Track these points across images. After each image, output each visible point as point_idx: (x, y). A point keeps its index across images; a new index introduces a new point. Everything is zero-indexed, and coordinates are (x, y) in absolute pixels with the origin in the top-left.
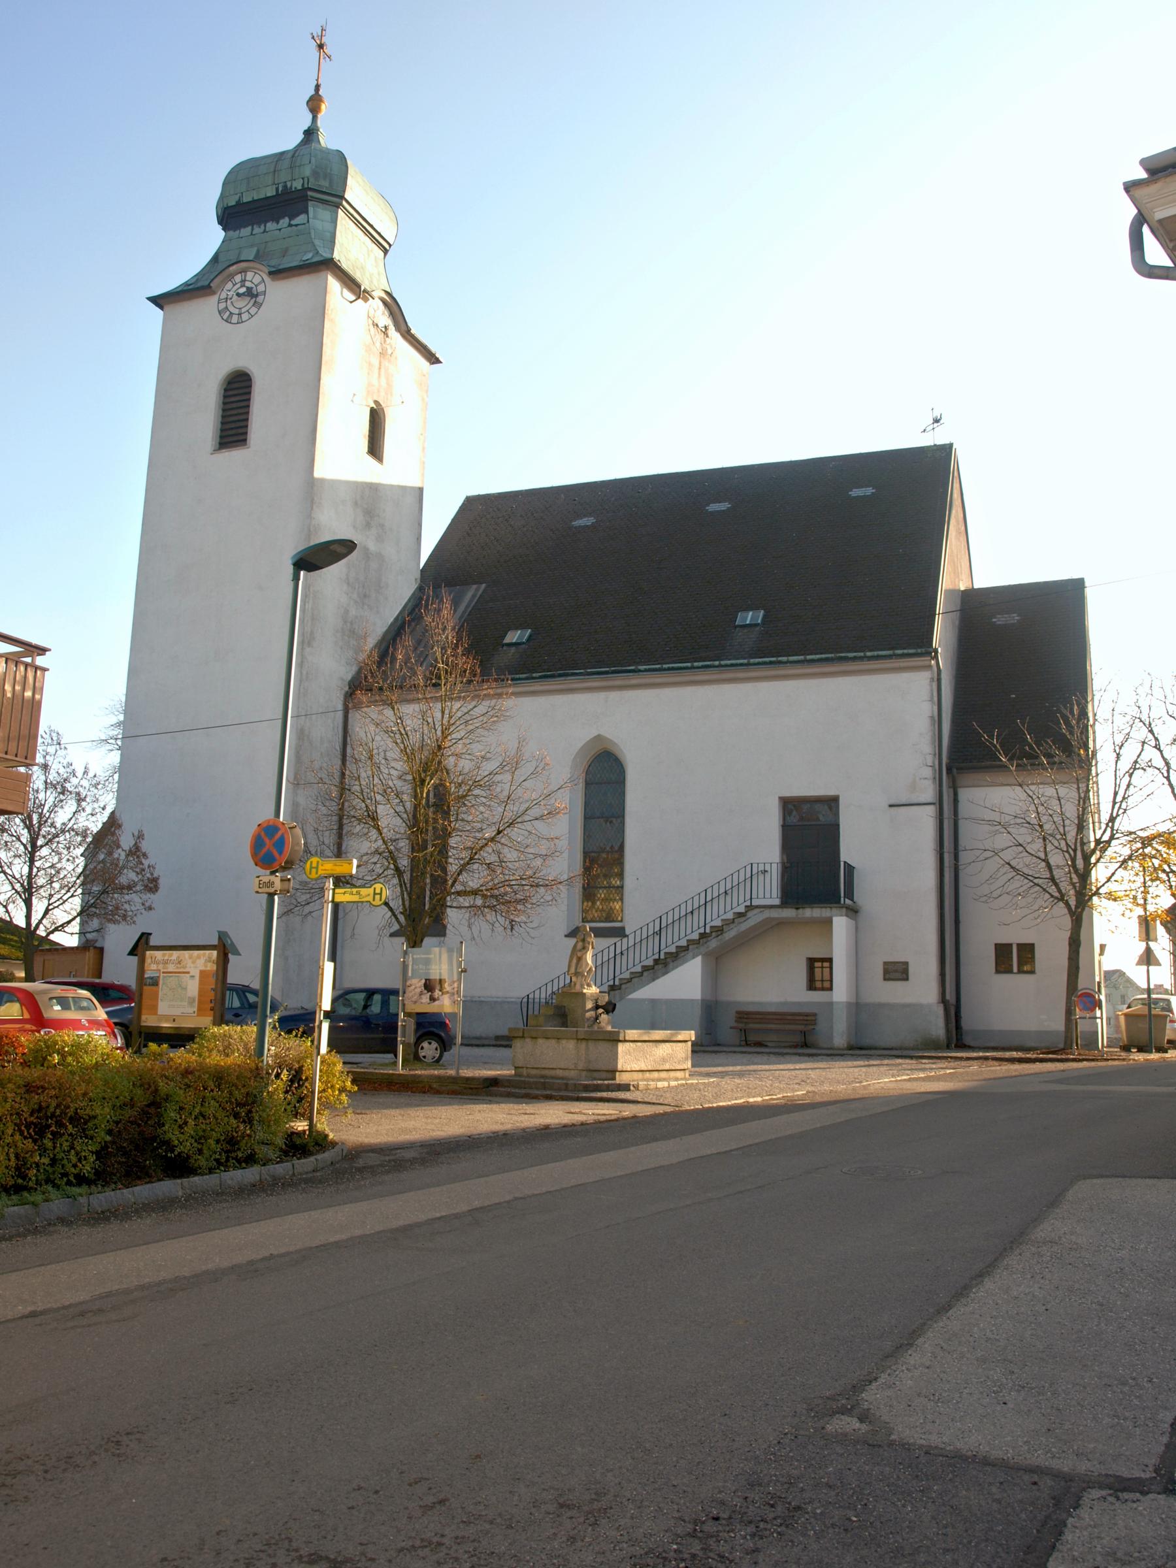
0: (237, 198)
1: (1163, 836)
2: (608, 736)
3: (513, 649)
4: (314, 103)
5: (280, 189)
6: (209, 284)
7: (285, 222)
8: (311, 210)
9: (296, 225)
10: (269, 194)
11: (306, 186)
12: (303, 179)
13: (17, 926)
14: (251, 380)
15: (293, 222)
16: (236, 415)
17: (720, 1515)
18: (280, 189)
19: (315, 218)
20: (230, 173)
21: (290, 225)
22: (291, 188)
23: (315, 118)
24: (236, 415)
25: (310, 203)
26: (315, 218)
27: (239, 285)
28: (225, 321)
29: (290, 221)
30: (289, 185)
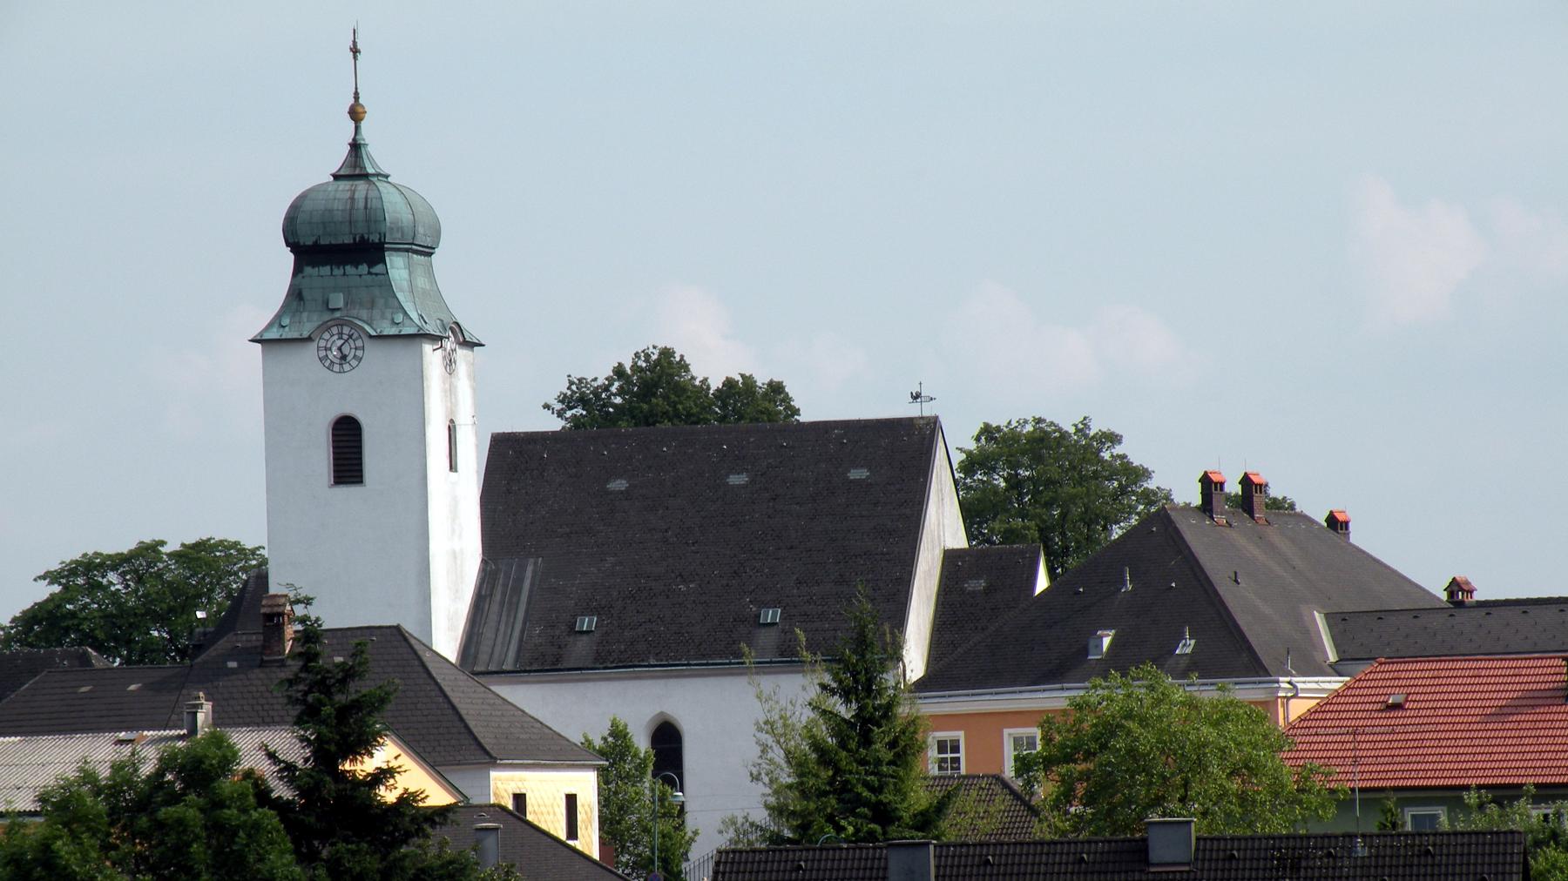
0: (314, 239)
1: (1029, 530)
2: (300, 192)
3: (585, 638)
4: (356, 114)
5: (357, 240)
6: (310, 336)
7: (364, 268)
8: (387, 259)
9: (376, 274)
10: (346, 242)
11: (383, 240)
12: (380, 234)
13: (61, 591)
14: (361, 429)
15: (372, 270)
16: (342, 441)
17: (391, 765)
18: (357, 240)
19: (392, 268)
20: (297, 198)
21: (369, 273)
22: (368, 239)
23: (357, 128)
24: (342, 441)
25: (386, 253)
26: (392, 268)
27: (336, 337)
28: (320, 359)
29: (369, 268)
30: (366, 237)
